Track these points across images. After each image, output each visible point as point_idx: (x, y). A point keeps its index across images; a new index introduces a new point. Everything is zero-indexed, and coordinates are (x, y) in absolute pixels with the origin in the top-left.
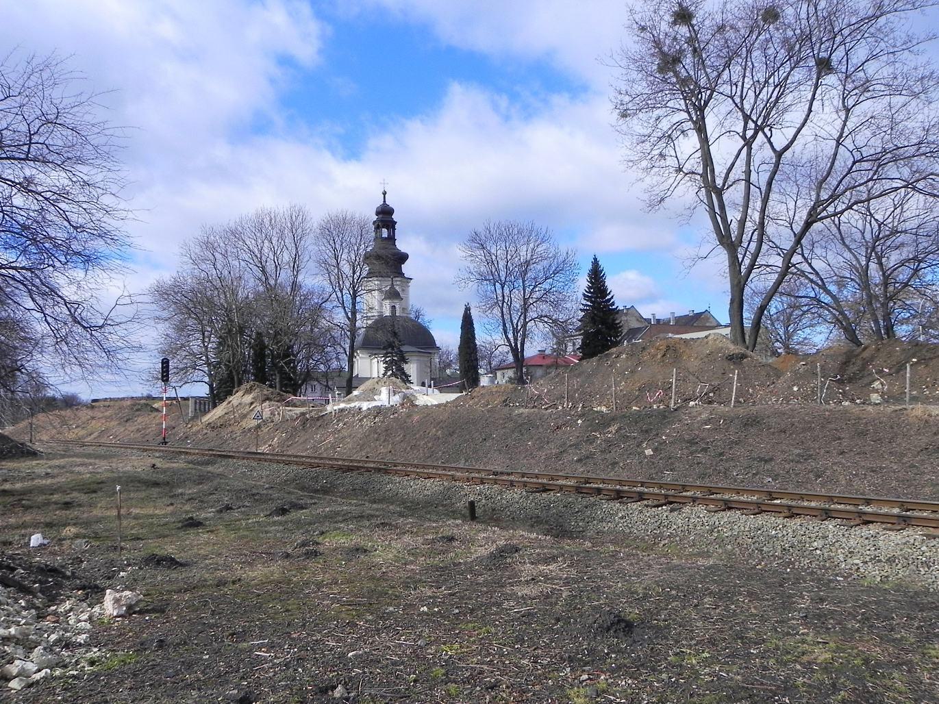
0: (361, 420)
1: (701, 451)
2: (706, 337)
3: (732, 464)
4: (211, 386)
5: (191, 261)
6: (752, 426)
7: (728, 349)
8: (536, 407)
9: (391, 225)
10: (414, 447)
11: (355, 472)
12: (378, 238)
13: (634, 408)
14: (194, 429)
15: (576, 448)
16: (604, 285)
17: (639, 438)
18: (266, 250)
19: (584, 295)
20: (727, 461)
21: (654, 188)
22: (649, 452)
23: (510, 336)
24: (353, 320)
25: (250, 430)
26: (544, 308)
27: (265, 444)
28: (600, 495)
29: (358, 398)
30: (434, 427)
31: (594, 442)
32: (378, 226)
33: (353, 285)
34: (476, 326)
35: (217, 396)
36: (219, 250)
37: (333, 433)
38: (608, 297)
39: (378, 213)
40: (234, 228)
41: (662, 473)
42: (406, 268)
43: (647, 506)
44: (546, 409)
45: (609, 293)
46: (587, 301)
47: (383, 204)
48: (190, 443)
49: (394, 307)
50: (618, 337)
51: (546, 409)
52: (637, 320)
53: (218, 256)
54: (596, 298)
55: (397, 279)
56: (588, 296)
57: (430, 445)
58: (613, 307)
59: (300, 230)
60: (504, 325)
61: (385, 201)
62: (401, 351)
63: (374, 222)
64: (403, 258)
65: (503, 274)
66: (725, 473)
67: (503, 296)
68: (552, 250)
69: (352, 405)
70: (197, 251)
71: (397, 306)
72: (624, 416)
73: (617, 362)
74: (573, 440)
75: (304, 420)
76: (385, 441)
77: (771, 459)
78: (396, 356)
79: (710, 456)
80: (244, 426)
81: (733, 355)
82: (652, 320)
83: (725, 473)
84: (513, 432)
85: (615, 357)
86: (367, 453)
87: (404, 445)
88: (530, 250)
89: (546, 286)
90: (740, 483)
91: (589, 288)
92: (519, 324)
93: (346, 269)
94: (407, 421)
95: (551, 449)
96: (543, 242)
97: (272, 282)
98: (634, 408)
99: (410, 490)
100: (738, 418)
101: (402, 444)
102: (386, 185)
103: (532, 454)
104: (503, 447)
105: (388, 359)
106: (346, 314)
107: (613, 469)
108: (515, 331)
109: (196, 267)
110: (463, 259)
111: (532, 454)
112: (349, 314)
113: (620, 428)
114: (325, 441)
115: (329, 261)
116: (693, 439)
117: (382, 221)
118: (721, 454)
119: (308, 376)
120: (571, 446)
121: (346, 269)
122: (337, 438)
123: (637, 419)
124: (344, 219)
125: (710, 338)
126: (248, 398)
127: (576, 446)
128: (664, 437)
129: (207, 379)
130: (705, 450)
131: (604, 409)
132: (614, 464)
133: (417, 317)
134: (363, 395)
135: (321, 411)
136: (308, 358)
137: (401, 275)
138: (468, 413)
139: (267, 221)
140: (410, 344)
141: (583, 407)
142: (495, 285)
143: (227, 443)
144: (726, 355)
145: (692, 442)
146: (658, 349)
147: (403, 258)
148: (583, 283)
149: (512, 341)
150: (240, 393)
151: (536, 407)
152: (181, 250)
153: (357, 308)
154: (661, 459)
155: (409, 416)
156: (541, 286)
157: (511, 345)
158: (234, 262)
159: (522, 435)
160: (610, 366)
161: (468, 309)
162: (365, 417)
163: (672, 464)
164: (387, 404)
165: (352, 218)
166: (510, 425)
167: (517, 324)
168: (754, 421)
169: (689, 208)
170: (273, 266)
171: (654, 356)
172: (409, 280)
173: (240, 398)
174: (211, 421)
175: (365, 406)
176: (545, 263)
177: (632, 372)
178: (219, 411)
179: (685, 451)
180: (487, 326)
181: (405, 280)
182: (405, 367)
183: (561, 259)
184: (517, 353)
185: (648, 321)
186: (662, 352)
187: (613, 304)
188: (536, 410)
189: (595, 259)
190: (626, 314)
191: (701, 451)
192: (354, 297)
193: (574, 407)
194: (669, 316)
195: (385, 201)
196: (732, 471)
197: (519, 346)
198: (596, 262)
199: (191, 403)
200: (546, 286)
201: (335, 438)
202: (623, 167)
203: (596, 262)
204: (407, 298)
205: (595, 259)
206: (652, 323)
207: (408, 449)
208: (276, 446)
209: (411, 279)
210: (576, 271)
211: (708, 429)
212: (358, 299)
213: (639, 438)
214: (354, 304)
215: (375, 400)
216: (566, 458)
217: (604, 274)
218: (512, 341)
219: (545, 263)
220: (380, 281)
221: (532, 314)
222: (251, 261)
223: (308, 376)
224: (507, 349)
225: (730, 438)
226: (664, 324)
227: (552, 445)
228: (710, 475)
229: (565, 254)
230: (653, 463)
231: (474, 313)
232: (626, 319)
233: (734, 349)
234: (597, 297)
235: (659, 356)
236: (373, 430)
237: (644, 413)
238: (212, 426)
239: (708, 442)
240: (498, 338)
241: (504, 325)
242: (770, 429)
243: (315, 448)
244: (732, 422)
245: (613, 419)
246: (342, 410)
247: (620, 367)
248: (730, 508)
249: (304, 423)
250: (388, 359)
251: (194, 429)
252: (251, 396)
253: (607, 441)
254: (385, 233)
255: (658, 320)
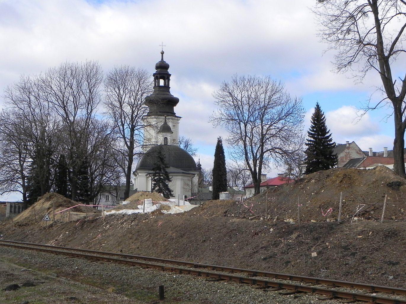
0: (122, 223)
1: (351, 255)
2: (374, 169)
3: (369, 265)
4: (24, 195)
5: (13, 101)
6: (391, 237)
7: (389, 178)
8: (245, 218)
9: (166, 76)
10: (155, 245)
11: (99, 262)
12: (157, 87)
13: (312, 221)
14: (7, 226)
15: (265, 250)
16: (324, 126)
17: (311, 244)
18: (67, 94)
19: (309, 133)
20: (366, 263)
21: (343, 55)
22: (314, 254)
23: (251, 162)
24: (131, 148)
25: (45, 228)
26: (277, 142)
27: (53, 239)
28: (255, 284)
29: (126, 207)
30: (171, 230)
31: (279, 245)
32: (157, 77)
33: (132, 120)
34: (226, 154)
35: (27, 203)
36: (33, 94)
37: (102, 232)
38: (327, 135)
39: (157, 68)
40: (44, 78)
41: (319, 270)
42: (177, 109)
43: (280, 294)
44: (252, 219)
45: (328, 132)
46: (311, 137)
47: (161, 61)
48: (3, 236)
49: (166, 139)
50: (334, 165)
51: (252, 219)
52: (357, 153)
53: (32, 98)
54: (318, 135)
55: (169, 117)
56: (311, 134)
57: (166, 243)
58: (331, 143)
59: (94, 80)
60: (246, 154)
61: (162, 59)
62: (166, 172)
63: (154, 75)
64: (174, 101)
65: (246, 116)
66: (363, 272)
67: (246, 132)
68: (284, 98)
69: (121, 212)
70: (17, 94)
71: (169, 138)
72: (304, 227)
73: (308, 186)
74: (265, 243)
75: (83, 222)
76: (136, 240)
77: (397, 263)
78: (162, 176)
79: (356, 259)
80: (41, 225)
81: (393, 182)
82: (370, 153)
83: (363, 272)
84: (225, 236)
85: (307, 182)
86: (123, 248)
87: (148, 243)
88: (267, 98)
89: (280, 125)
90: (371, 280)
91: (313, 127)
92: (258, 154)
93: (127, 109)
94: (154, 225)
95: (248, 250)
96: (276, 92)
97: (71, 118)
98: (312, 221)
99: (130, 276)
100: (383, 231)
101: (147, 242)
102: (164, 47)
103: (234, 253)
104: (216, 247)
105: (156, 178)
106: (126, 143)
107: (286, 266)
108: (255, 160)
109: (16, 106)
110: (216, 103)
111: (234, 253)
112: (129, 144)
113: (299, 236)
114: (95, 238)
115: (114, 103)
116: (347, 246)
117: (159, 74)
118: (364, 258)
119: (102, 188)
120: (262, 248)
121: (127, 109)
122: (104, 236)
123: (312, 229)
124: (127, 72)
125: (377, 169)
126: (47, 205)
127: (265, 248)
128: (327, 244)
129: (21, 189)
130: (353, 254)
131: (291, 221)
132: (288, 262)
133: (186, 146)
134: (129, 205)
135: (97, 216)
136: (102, 175)
137: (173, 114)
138: (196, 221)
139: (69, 72)
140: (177, 167)
141: (278, 219)
142: (240, 124)
143: (28, 237)
144: (388, 183)
145: (346, 248)
146: (337, 177)
147: (174, 101)
148: (308, 123)
149: (252, 166)
150: (42, 201)
151: (245, 218)
152: (6, 94)
153: (134, 139)
154: (321, 260)
155: (156, 221)
156: (275, 125)
157: (251, 170)
158: (44, 103)
159: (231, 238)
160: (302, 188)
161: (220, 141)
162: (126, 221)
163: (329, 264)
164: (142, 212)
165: (132, 72)
166: (224, 231)
167: (256, 154)
168: (393, 233)
169: (362, 71)
170: (73, 106)
171: (334, 182)
172: (179, 119)
173: (41, 204)
174: (19, 220)
175: (130, 212)
176: (279, 108)
177: (316, 193)
178: (26, 214)
179: (340, 255)
180: (233, 155)
181: (176, 118)
182: (170, 185)
183: (291, 105)
184: (256, 176)
185: (366, 153)
186: (340, 179)
187: (331, 140)
188: (244, 220)
189: (318, 106)
190: (348, 148)
191: (351, 255)
192: (132, 130)
193: (272, 219)
194: (383, 150)
195: (162, 59)
196: (368, 271)
197: (257, 171)
198: (318, 109)
199: (8, 206)
200: (280, 125)
201: (103, 236)
202: (319, 39)
203: (318, 109)
204: (177, 132)
205: (318, 106)
206: (370, 155)
207: (151, 246)
208: (61, 240)
209: (181, 117)
210: (303, 114)
211: (360, 239)
212: (136, 132)
213: (311, 244)
214: (132, 136)
215: (138, 209)
216: (257, 256)
217: (324, 118)
218: (252, 166)
219: (279, 108)
220: (156, 118)
221: (268, 146)
222: (57, 103)
223: (102, 188)
224: (248, 173)
225: (373, 246)
226: (379, 156)
227: (249, 247)
228: (352, 274)
229: (294, 101)
230: (315, 263)
231: (225, 146)
232: (348, 151)
233: (394, 178)
234: (318, 135)
235: (338, 182)
236: (129, 231)
237: (318, 225)
238: (20, 225)
239: (357, 249)
240: (242, 163)
241: (246, 154)
242: (403, 240)
243: (87, 243)
244: (377, 234)
245: (296, 229)
246: (112, 215)
247: (310, 189)
248: (336, 298)
249: (82, 225)
250: (156, 178)
251: (7, 226)
252: (50, 203)
253: (288, 245)
254: (162, 82)
255: (374, 154)
